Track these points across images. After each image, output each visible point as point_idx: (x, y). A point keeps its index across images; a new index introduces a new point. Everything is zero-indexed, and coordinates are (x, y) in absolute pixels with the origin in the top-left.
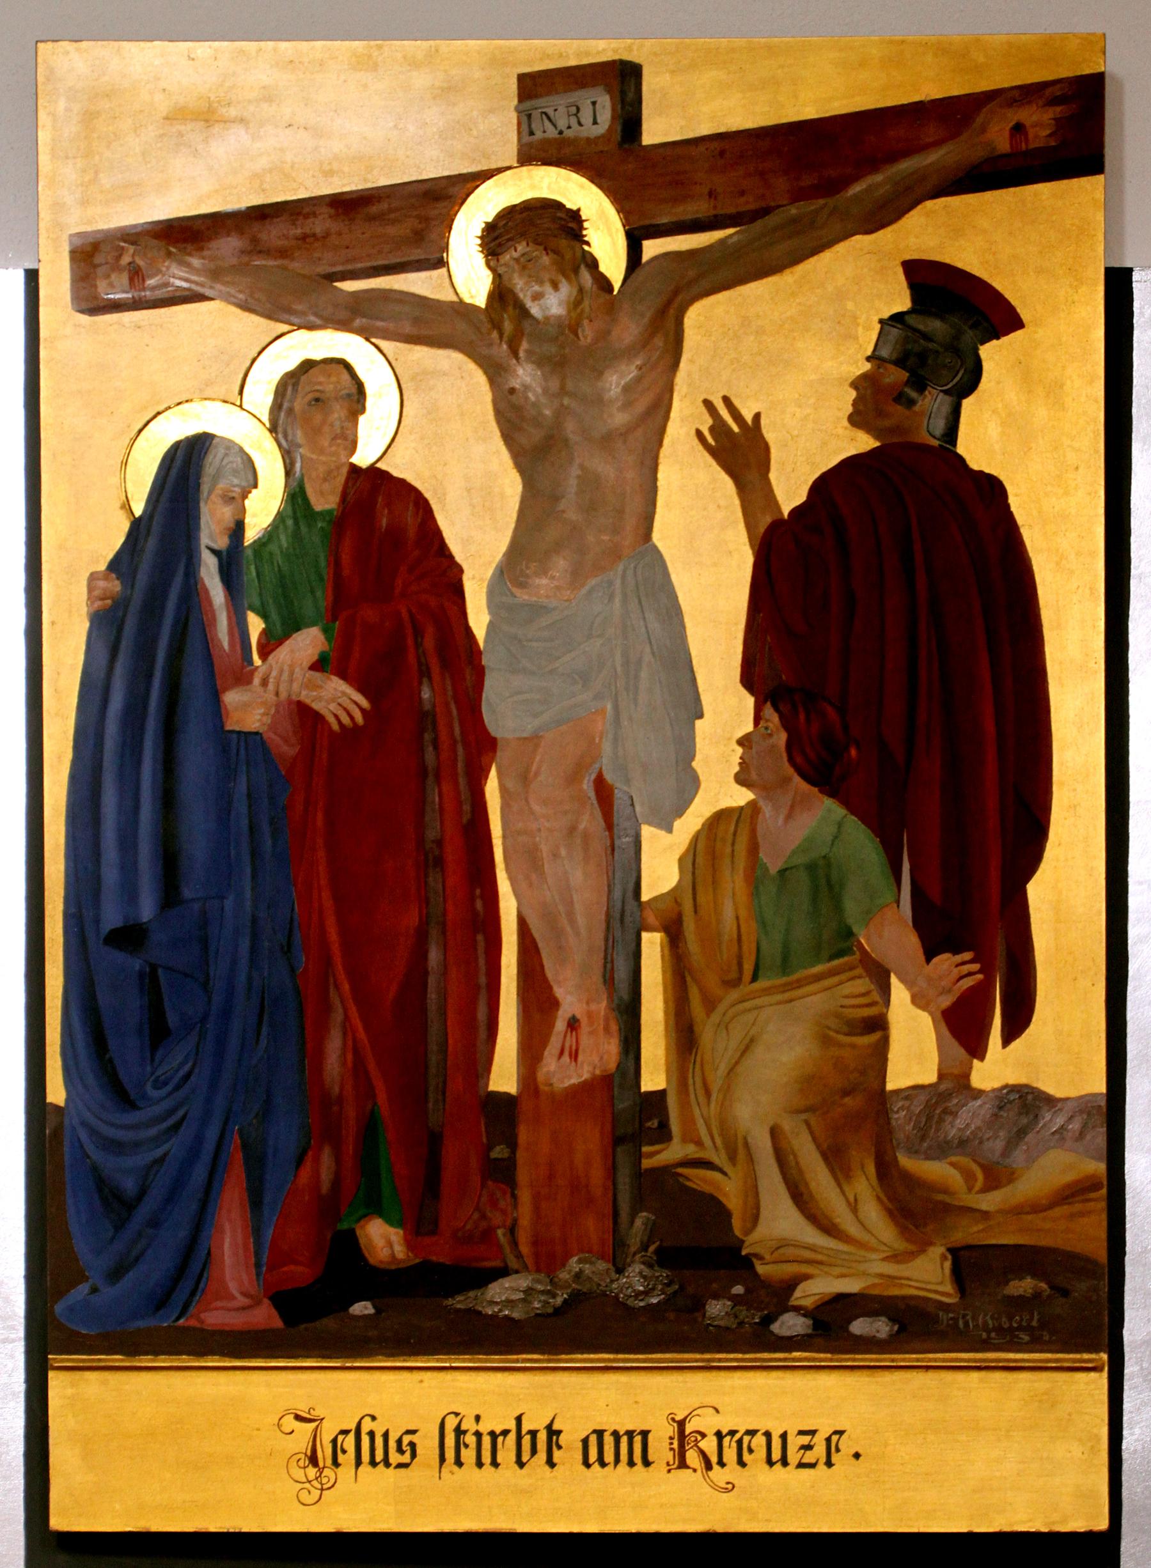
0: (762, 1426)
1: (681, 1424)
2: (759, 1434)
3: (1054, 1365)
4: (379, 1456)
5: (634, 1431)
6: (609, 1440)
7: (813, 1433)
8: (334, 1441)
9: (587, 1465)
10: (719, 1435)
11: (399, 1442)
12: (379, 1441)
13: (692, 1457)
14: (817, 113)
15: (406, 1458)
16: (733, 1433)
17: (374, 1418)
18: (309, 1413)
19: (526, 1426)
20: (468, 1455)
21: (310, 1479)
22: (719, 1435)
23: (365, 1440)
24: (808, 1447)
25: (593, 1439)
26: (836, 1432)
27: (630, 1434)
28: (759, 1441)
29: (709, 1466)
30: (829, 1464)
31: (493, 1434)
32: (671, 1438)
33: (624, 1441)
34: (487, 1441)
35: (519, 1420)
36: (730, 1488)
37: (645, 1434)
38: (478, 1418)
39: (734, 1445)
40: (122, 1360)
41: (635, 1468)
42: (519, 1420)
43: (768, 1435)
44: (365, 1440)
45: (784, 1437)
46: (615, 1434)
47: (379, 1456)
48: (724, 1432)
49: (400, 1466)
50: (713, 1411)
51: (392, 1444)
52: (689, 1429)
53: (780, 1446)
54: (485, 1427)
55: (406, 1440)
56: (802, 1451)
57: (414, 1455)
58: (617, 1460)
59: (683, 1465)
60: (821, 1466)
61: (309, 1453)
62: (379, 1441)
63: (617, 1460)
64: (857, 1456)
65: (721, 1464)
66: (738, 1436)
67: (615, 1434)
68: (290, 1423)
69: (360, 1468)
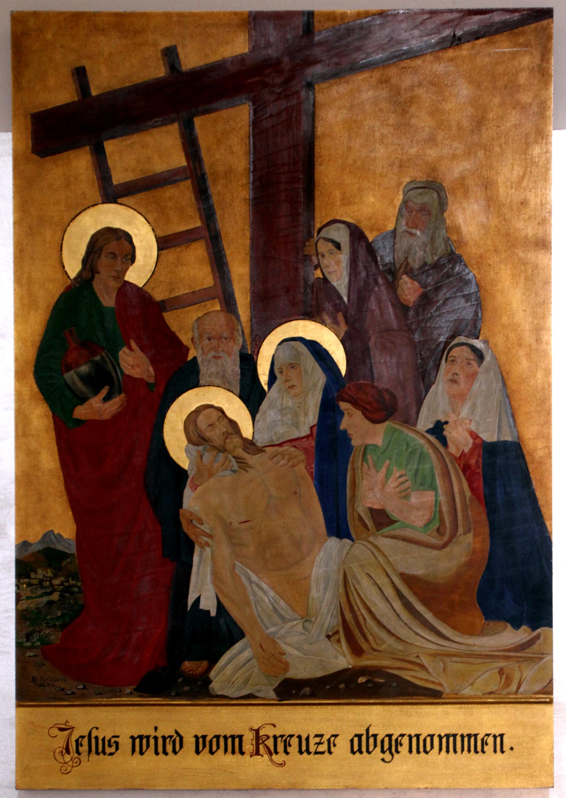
0: (407, 732)
1: (257, 731)
2: (295, 736)
3: (491, 700)
4: (100, 749)
5: (143, 736)
6: (459, 739)
7: (322, 736)
8: (77, 741)
9: (353, 752)
10: (275, 737)
11: (109, 741)
12: (100, 742)
13: (262, 748)
14: (9, 155)
15: (113, 749)
16: (282, 736)
17: (97, 728)
18: (66, 725)
19: (371, 732)
20: (169, 748)
21: (67, 761)
22: (275, 737)
23: (93, 741)
24: (319, 744)
25: (356, 740)
26: (332, 736)
27: (448, 736)
28: (294, 741)
29: (271, 754)
30: (330, 752)
31: (164, 738)
32: (252, 740)
33: (466, 739)
34: (160, 741)
35: (367, 730)
36: (282, 765)
37: (476, 736)
38: (156, 728)
39: (283, 743)
40: (162, 701)
41: (159, 755)
42: (367, 730)
43: (300, 737)
44: (93, 741)
45: (307, 739)
46: (440, 737)
47: (100, 749)
48: (228, 736)
49: (111, 754)
50: (272, 727)
51: (107, 743)
52: (261, 733)
53: (159, 746)
54: (159, 734)
55: (113, 740)
56: (316, 746)
57: (117, 749)
58: (463, 750)
59: (257, 753)
60: (327, 754)
61: (65, 747)
62: (100, 742)
63: (463, 750)
64: (512, 749)
65: (276, 753)
66: (284, 738)
67: (440, 737)
68: (55, 731)
69: (91, 755)
